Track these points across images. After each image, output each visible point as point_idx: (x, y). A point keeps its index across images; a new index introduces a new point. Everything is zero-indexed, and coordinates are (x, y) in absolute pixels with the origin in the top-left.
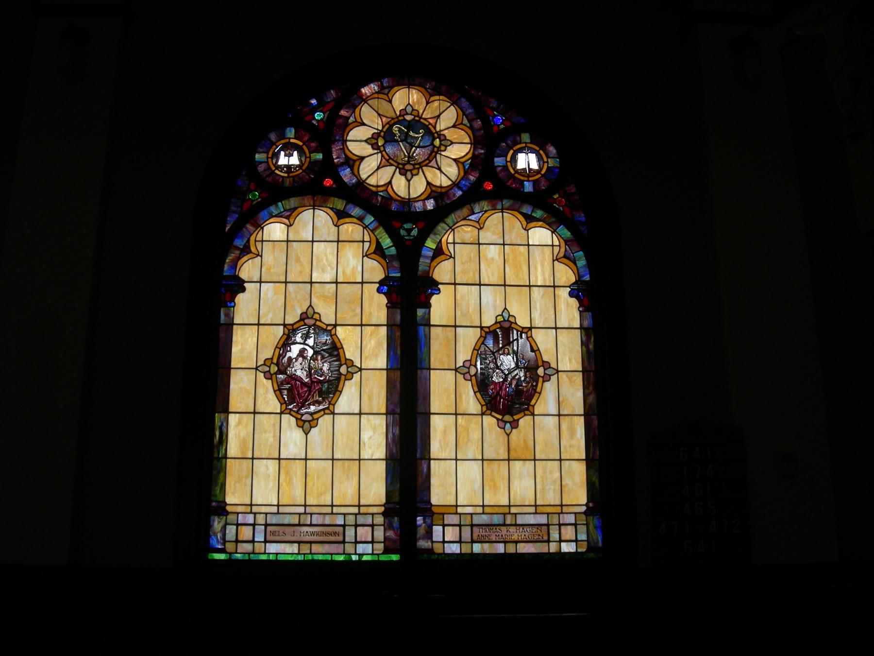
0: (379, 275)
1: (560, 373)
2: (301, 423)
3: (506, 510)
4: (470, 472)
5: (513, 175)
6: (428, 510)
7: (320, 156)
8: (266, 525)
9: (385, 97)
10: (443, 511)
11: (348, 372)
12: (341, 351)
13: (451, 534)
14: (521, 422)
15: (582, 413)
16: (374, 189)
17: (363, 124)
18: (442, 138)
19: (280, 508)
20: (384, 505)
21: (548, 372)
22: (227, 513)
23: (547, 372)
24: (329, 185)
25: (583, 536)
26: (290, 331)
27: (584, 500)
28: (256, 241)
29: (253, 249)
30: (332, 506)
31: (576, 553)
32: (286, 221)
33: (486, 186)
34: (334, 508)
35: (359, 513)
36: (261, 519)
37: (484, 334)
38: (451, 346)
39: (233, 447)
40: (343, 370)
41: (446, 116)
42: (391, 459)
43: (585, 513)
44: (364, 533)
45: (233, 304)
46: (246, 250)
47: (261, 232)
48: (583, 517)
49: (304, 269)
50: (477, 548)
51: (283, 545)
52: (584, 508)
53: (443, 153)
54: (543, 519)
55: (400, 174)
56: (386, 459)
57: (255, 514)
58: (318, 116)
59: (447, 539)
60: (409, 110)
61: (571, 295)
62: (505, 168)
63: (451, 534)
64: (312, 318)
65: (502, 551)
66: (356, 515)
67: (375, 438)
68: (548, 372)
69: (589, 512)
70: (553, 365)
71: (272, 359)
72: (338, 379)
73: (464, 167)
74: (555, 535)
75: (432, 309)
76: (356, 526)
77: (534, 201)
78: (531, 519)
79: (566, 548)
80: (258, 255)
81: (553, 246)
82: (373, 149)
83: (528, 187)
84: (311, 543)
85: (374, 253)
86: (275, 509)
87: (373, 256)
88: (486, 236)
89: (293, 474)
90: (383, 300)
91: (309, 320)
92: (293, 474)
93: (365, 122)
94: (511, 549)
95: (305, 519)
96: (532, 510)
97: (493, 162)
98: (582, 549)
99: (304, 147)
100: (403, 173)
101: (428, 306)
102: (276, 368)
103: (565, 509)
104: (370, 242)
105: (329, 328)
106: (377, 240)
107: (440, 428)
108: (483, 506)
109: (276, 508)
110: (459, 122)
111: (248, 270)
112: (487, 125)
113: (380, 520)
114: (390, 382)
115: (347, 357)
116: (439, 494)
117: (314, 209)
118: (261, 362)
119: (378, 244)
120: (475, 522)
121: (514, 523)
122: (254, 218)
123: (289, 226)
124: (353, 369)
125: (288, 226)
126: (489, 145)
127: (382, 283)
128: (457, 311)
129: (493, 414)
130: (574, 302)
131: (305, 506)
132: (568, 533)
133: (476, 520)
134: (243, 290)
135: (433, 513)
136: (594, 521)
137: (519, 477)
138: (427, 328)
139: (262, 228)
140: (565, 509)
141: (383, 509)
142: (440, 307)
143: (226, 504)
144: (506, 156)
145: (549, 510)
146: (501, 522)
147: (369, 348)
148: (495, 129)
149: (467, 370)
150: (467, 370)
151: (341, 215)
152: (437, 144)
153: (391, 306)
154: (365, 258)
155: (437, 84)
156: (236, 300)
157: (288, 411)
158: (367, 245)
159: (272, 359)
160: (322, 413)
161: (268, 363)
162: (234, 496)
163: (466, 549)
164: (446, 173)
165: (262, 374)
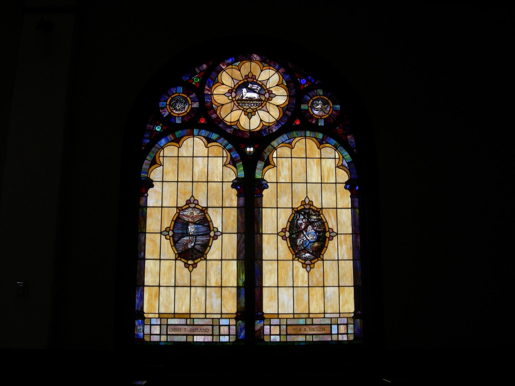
2: (305, 266)
3: (188, 316)
4: (286, 295)
5: (330, 115)
6: (262, 317)
7: (196, 105)
10: (270, 317)
12: (211, 223)
13: (276, 330)
15: (352, 259)
20: (235, 314)
21: (283, 234)
22: (144, 318)
23: (284, 234)
24: (206, 122)
25: (351, 331)
27: (352, 309)
28: (227, 157)
30: (294, 314)
32: (177, 145)
33: (294, 122)
36: (284, 322)
37: (294, 212)
38: (274, 219)
39: (149, 279)
43: (353, 317)
45: (146, 195)
46: (154, 162)
49: (188, 173)
50: (290, 339)
53: (270, 102)
59: (273, 334)
60: (250, 76)
63: (276, 330)
64: (193, 203)
67: (231, 274)
68: (283, 234)
70: (335, 230)
71: (170, 227)
74: (334, 331)
76: (160, 325)
77: (329, 133)
80: (161, 165)
81: (163, 157)
83: (321, 123)
84: (312, 335)
85: (270, 164)
86: (292, 316)
89: (181, 296)
90: (349, 193)
91: (192, 203)
92: (181, 296)
98: (351, 338)
104: (273, 158)
108: (294, 314)
110: (280, 83)
111: (155, 174)
112: (297, 85)
113: (351, 321)
114: (354, 242)
116: (268, 307)
117: (306, 138)
118: (280, 230)
120: (289, 323)
121: (192, 323)
125: (179, 148)
127: (346, 183)
129: (182, 259)
130: (234, 191)
132: (342, 329)
134: (267, 187)
135: (145, 318)
137: (315, 296)
140: (223, 316)
143: (264, 314)
144: (308, 104)
147: (225, 219)
148: (302, 88)
151: (321, 143)
156: (263, 193)
158: (225, 159)
163: (283, 339)
164: (270, 115)
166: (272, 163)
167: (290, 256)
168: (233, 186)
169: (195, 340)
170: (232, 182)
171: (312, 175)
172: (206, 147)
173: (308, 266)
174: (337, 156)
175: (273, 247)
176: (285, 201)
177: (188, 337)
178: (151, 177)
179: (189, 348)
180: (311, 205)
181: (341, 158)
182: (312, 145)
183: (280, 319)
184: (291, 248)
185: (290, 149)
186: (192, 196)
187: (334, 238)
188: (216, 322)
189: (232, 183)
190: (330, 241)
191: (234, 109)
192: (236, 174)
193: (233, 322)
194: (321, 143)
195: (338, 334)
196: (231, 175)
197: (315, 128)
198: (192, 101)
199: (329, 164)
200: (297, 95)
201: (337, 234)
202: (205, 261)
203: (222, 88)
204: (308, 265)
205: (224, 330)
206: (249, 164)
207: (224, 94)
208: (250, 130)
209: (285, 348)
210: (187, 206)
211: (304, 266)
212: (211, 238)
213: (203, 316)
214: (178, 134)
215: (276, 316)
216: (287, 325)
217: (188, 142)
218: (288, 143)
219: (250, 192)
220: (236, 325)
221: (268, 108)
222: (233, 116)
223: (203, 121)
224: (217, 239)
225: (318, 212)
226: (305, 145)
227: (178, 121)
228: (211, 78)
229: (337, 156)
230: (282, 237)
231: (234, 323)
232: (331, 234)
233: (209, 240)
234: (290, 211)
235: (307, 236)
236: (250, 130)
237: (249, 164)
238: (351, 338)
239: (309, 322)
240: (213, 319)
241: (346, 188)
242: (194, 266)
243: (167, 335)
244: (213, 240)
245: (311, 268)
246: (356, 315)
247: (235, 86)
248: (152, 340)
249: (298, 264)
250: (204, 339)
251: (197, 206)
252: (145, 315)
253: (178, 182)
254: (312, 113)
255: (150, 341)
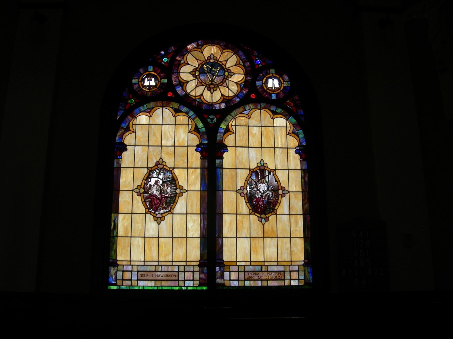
0: (197, 142)
1: (290, 193)
2: (156, 219)
3: (262, 264)
4: (244, 244)
5: (266, 91)
6: (222, 264)
7: (166, 81)
8: (138, 271)
9: (200, 50)
10: (230, 264)
11: (180, 192)
12: (177, 181)
13: (234, 276)
14: (270, 218)
15: (302, 213)
16: (194, 98)
17: (188, 64)
18: (229, 71)
19: (145, 262)
20: (199, 261)
21: (284, 192)
22: (118, 265)
23: (283, 192)
24: (170, 96)
25: (302, 277)
26: (150, 171)
27: (302, 258)
28: (133, 125)
29: (131, 129)
30: (172, 261)
31: (299, 286)
32: (148, 114)
33: (252, 96)
34: (173, 263)
35: (186, 265)
36: (135, 268)
37: (251, 173)
38: (234, 179)
39: (121, 231)
40: (178, 191)
41: (231, 60)
42: (202, 237)
43: (303, 265)
44: (189, 275)
45: (121, 157)
46: (128, 129)
47: (135, 120)
48: (302, 267)
49: (157, 139)
50: (247, 283)
51: (147, 281)
52: (303, 263)
53: (230, 79)
54: (281, 268)
55: (208, 90)
56: (200, 237)
57: (132, 265)
58: (165, 60)
59: (232, 279)
60: (212, 57)
61: (296, 152)
62: (262, 87)
63: (234, 276)
64: (162, 164)
65: (260, 285)
66: (184, 266)
67: (195, 227)
68: (284, 192)
69: (305, 265)
70: (287, 189)
71: (141, 185)
72: (175, 196)
73: (241, 86)
74: (288, 277)
75: (224, 160)
76: (185, 272)
77: (277, 104)
78: (275, 268)
79: (293, 283)
80: (134, 132)
81: (286, 127)
82: (194, 77)
83: (274, 97)
84: (161, 280)
85: (194, 131)
86: (142, 263)
87: (194, 132)
88: (252, 122)
89: (152, 245)
90: (199, 155)
91: (160, 165)
92: (152, 245)
93: (189, 63)
94: (265, 284)
95: (158, 268)
96: (276, 263)
97: (256, 84)
98: (302, 284)
99: (158, 76)
100: (209, 89)
101: (222, 158)
102: (143, 190)
103: (293, 263)
104: (192, 125)
105: (171, 169)
106: (196, 124)
107: (228, 221)
108: (250, 262)
109: (143, 262)
110: (238, 63)
111: (128, 139)
112: (253, 64)
113: (197, 268)
114: (202, 198)
115: (180, 184)
116: (228, 255)
117: (163, 108)
118: (135, 187)
119: (196, 126)
120: (246, 270)
121: (266, 270)
122: (131, 113)
123: (150, 117)
124: (183, 191)
125: (149, 117)
127: (198, 146)
128: (237, 161)
129: (256, 214)
130: (298, 156)
131: (158, 261)
132: (295, 275)
133: (247, 269)
134: (126, 150)
135: (225, 265)
136: (308, 269)
137: (269, 246)
138: (221, 170)
139: (136, 118)
140: (293, 263)
141: (198, 263)
142: (228, 159)
143: (117, 261)
144: (262, 81)
145: (285, 263)
146: (260, 270)
147: (191, 180)
148: (257, 67)
149: (242, 191)
150: (242, 191)
151: (177, 111)
153: (203, 158)
154: (189, 133)
155: (226, 44)
156: (122, 155)
157: (149, 212)
158: (190, 127)
159: (141, 185)
160: (167, 213)
161: (139, 188)
162: (121, 256)
163: (242, 284)
164: (231, 89)
165: (136, 194)
194: (177, 111)
200: (254, 75)
219: (212, 151)
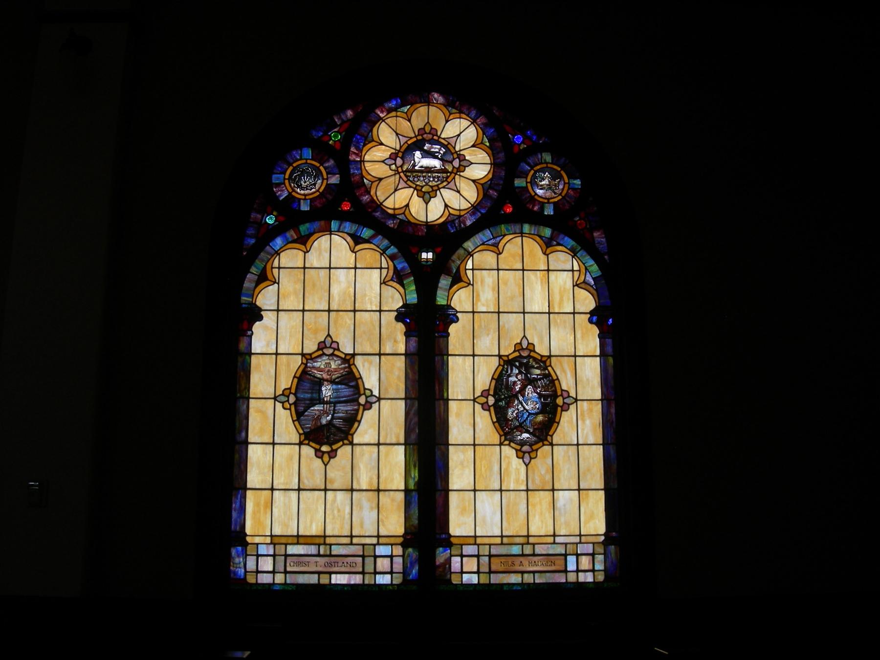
2: (521, 454)
3: (321, 541)
4: (488, 504)
5: (563, 197)
6: (447, 542)
7: (335, 180)
10: (462, 542)
12: (360, 381)
13: (471, 565)
15: (601, 442)
20: (402, 536)
21: (483, 400)
22: (247, 544)
23: (485, 400)
24: (351, 208)
25: (599, 566)
27: (602, 529)
28: (388, 268)
30: (502, 536)
32: (303, 248)
33: (503, 209)
36: (485, 550)
37: (502, 363)
38: (467, 375)
39: (255, 477)
43: (603, 543)
45: (249, 333)
46: (263, 278)
49: (321, 297)
50: (496, 579)
53: (462, 174)
59: (467, 571)
60: (427, 129)
63: (471, 565)
64: (330, 347)
67: (395, 468)
68: (483, 400)
70: (573, 394)
71: (290, 389)
74: (572, 566)
76: (274, 556)
77: (562, 227)
80: (275, 282)
81: (279, 268)
83: (549, 211)
84: (534, 572)
85: (462, 281)
86: (498, 540)
89: (309, 506)
90: (596, 331)
91: (327, 346)
92: (309, 506)
98: (601, 577)
104: (466, 269)
108: (502, 536)
110: (479, 141)
111: (265, 298)
112: (508, 146)
113: (600, 549)
114: (605, 414)
116: (459, 524)
117: (522, 236)
118: (478, 394)
120: (493, 552)
121: (328, 553)
125: (305, 253)
126: (507, 163)
127: (592, 313)
129: (311, 443)
130: (401, 327)
132: (585, 562)
134: (457, 320)
135: (247, 544)
137: (538, 506)
140: (382, 540)
143: (450, 536)
144: (526, 178)
147: (384, 375)
148: (516, 150)
151: (548, 245)
152: (454, 163)
156: (449, 331)
158: (384, 272)
163: (484, 580)
164: (461, 197)
166: (465, 279)
167: (496, 438)
168: (398, 319)
169: (333, 582)
170: (397, 311)
171: (533, 299)
172: (353, 251)
173: (527, 455)
174: (576, 267)
175: (467, 423)
176: (487, 344)
177: (321, 576)
178: (258, 303)
179: (322, 595)
180: (531, 351)
181: (583, 270)
182: (533, 247)
183: (478, 545)
184: (497, 424)
185: (495, 255)
186: (329, 335)
187: (571, 407)
188: (369, 551)
189: (396, 313)
190: (563, 413)
191: (400, 187)
192: (404, 297)
193: (398, 550)
194: (548, 245)
195: (578, 571)
196: (395, 299)
197: (538, 219)
198: (327, 173)
199: (563, 281)
201: (576, 400)
202: (350, 447)
203: (379, 150)
204: (526, 452)
205: (383, 564)
206: (426, 280)
207: (383, 162)
208: (427, 222)
209: (487, 595)
210: (320, 352)
211: (520, 454)
212: (361, 408)
213: (347, 540)
214: (304, 229)
215: (472, 541)
216: (490, 556)
217: (322, 243)
218: (493, 245)
219: (427, 328)
220: (403, 556)
221: (458, 184)
222: (397, 198)
223: (346, 207)
224: (370, 408)
225: (544, 362)
226: (521, 247)
227: (305, 207)
228: (361, 133)
229: (576, 267)
230: (482, 405)
231: (401, 553)
232: (565, 401)
233: (357, 410)
234: (495, 362)
235: (525, 403)
236: (427, 222)
237: (426, 280)
238: (601, 577)
239: (528, 550)
240: (363, 545)
241: (590, 321)
242: (332, 454)
243: (286, 572)
244: (364, 410)
245: (531, 458)
246: (609, 539)
247: (401, 147)
248: (259, 581)
249: (509, 452)
250: (349, 579)
251: (336, 353)
252: (249, 539)
253: (303, 311)
254: (533, 194)
255: (257, 584)
